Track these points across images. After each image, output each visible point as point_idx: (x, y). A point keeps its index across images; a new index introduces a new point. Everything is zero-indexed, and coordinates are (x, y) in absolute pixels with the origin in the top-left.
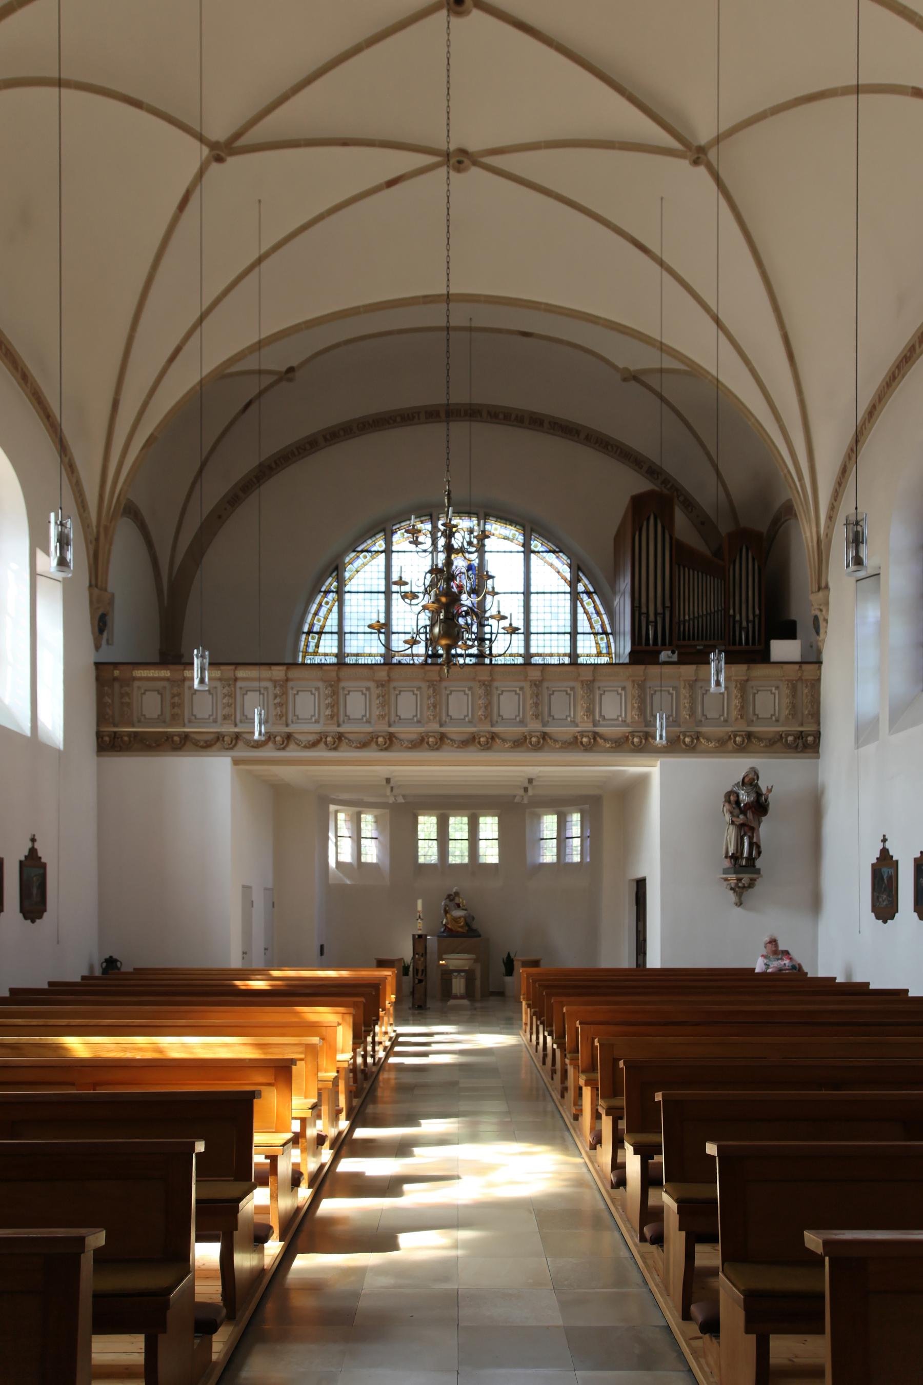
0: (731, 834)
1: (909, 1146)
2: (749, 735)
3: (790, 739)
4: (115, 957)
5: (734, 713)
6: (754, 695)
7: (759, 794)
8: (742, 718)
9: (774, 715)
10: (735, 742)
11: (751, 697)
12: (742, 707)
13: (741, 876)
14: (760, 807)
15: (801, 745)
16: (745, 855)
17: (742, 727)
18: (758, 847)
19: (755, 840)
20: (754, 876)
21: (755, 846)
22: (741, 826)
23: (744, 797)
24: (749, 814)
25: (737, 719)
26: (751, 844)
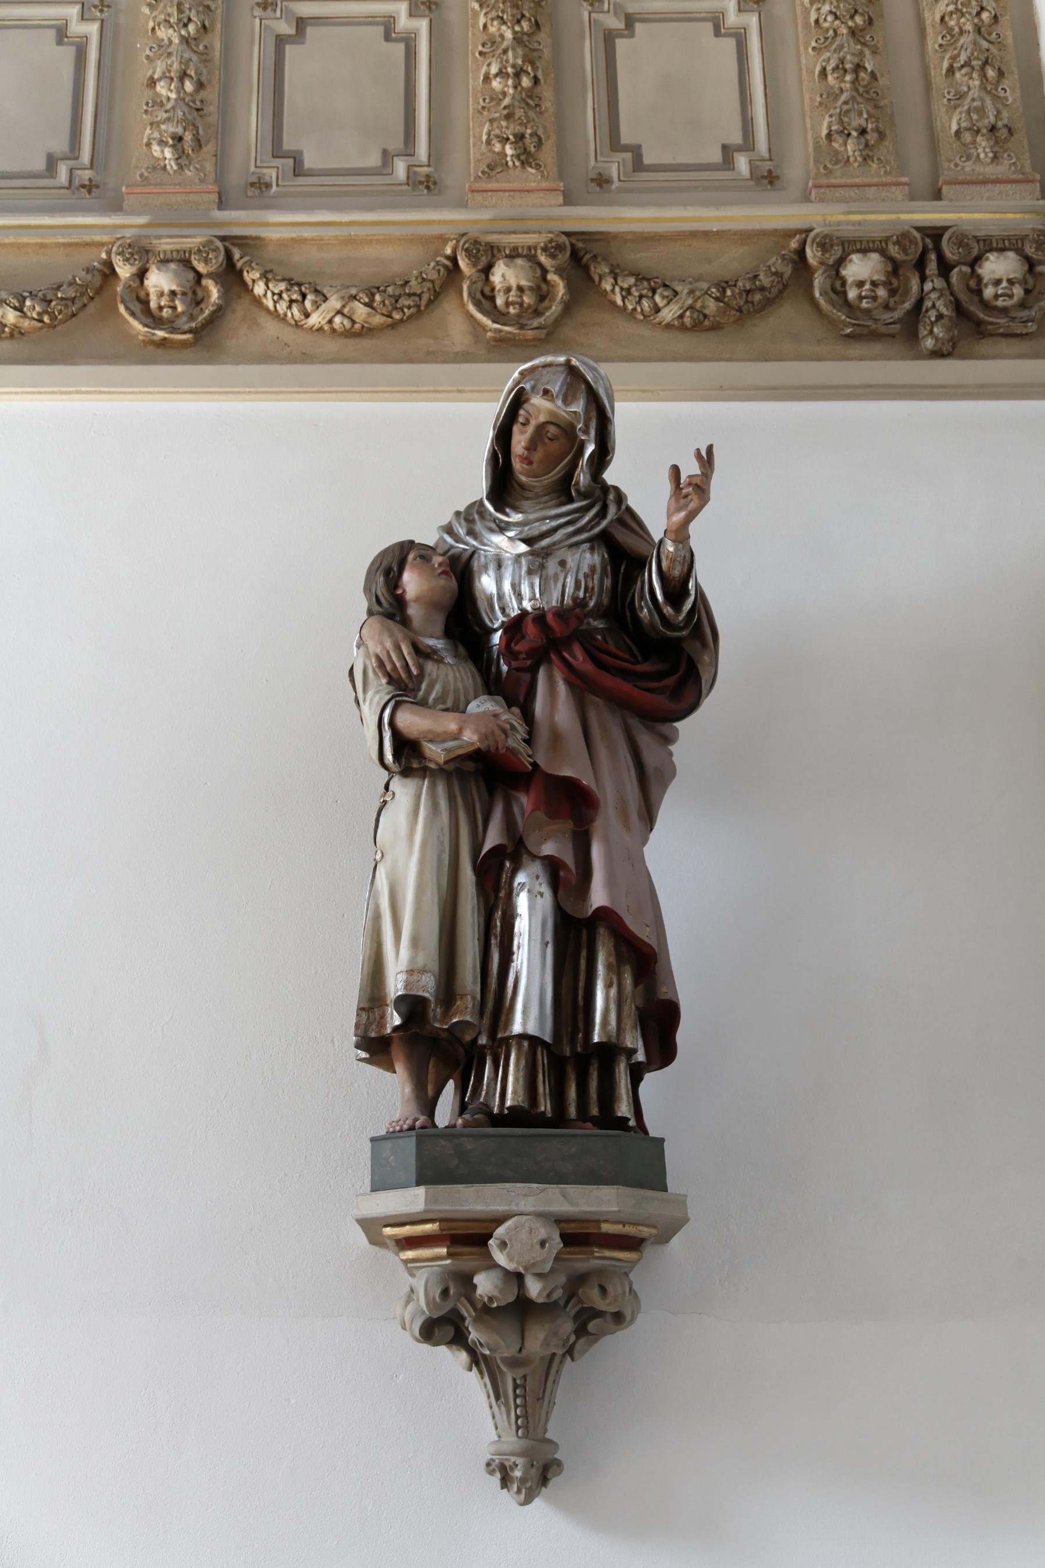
0: (406, 836)
1: (526, 362)
2: (580, 258)
3: (860, 268)
4: (507, 1499)
5: (476, 136)
6: (609, 38)
7: (622, 550)
8: (526, 158)
9: (748, 144)
10: (485, 298)
11: (588, 55)
12: (530, 99)
13: (474, 1200)
14: (641, 644)
15: (938, 304)
16: (528, 1013)
17: (537, 211)
18: (643, 961)
19: (598, 897)
20: (602, 1202)
21: (609, 940)
22: (483, 777)
23: (508, 585)
24: (554, 701)
25: (495, 166)
26: (574, 935)
